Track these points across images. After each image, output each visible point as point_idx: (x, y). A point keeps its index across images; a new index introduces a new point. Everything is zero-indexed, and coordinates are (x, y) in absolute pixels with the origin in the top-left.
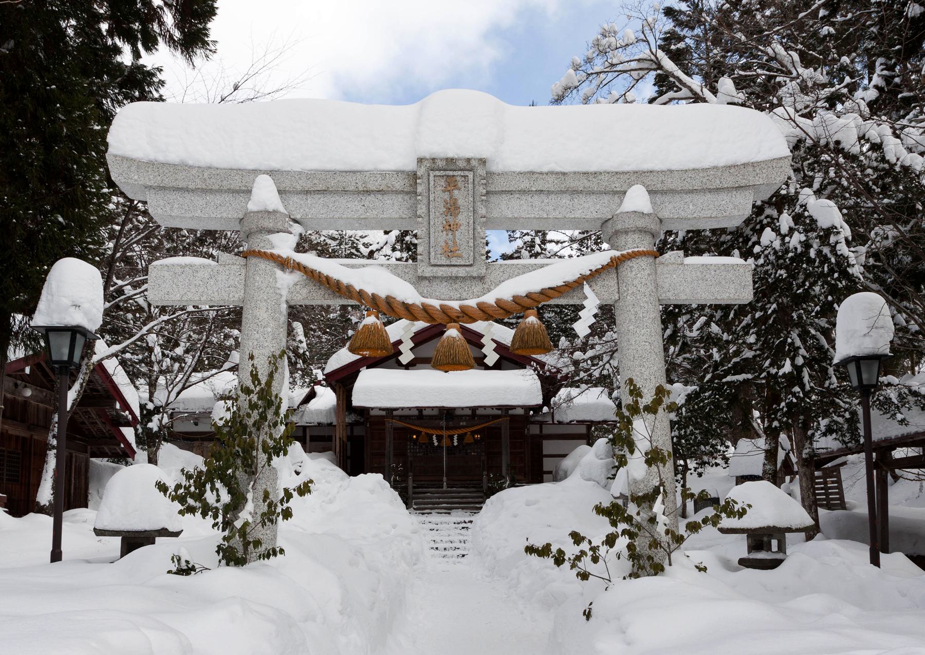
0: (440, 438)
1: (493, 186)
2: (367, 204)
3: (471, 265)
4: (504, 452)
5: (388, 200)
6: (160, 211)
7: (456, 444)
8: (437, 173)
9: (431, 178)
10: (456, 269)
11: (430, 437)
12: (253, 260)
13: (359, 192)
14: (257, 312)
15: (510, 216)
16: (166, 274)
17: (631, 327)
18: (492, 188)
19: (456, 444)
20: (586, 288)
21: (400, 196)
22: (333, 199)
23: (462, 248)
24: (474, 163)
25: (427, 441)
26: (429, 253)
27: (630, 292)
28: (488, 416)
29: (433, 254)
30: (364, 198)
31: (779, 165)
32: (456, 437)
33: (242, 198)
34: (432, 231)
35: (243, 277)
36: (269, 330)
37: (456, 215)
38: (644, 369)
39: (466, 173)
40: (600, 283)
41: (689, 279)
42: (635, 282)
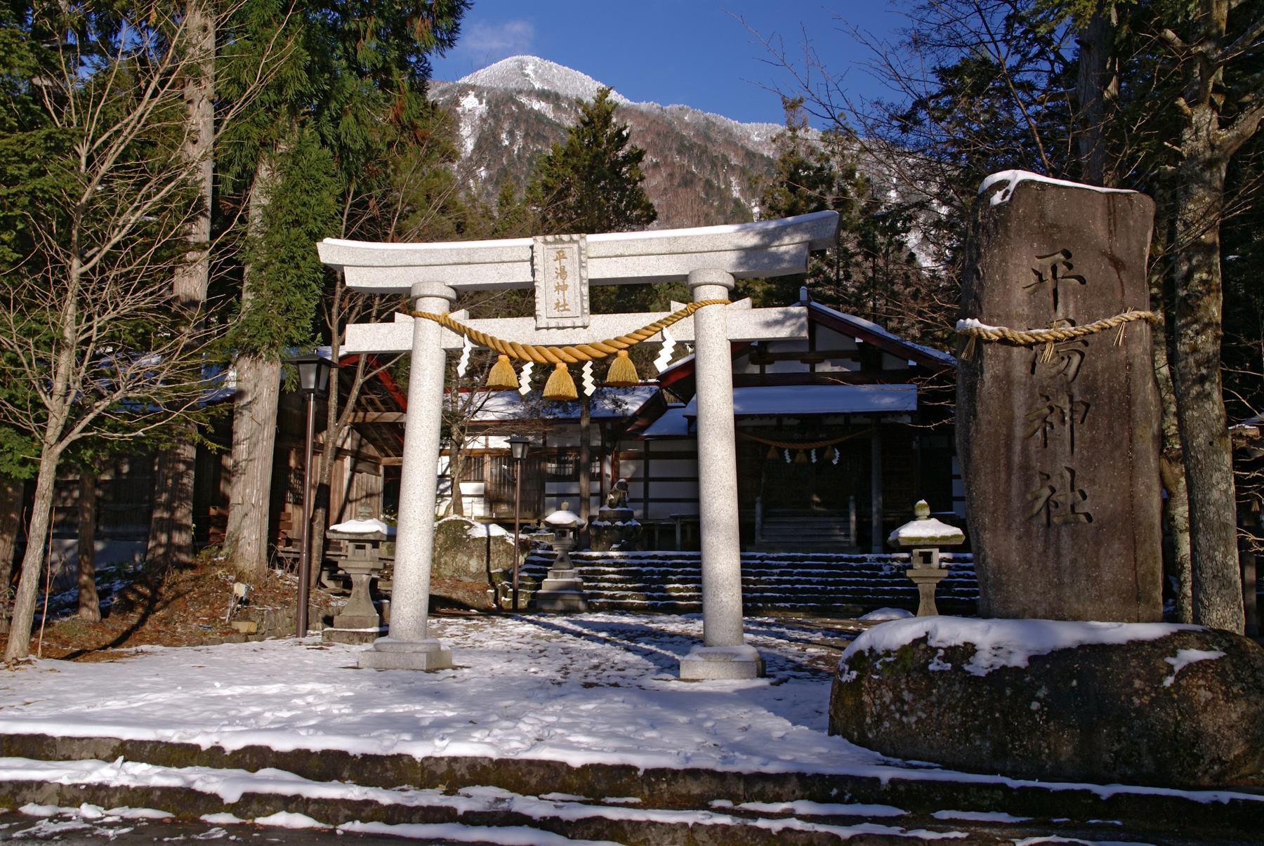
7: (814, 460)
19: (814, 460)
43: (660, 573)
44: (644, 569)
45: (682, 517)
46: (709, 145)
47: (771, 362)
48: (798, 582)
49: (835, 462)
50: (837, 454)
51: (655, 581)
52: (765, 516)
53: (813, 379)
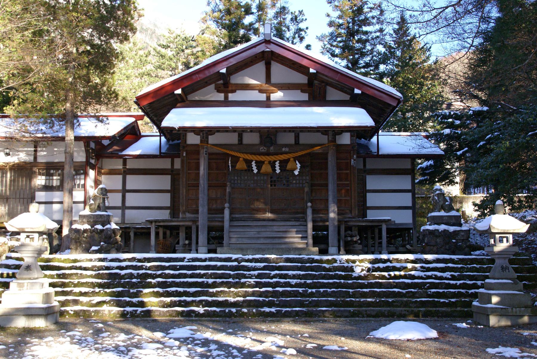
0: (259, 164)
7: (278, 171)
11: (248, 162)
19: (278, 171)
43: (139, 276)
44: (123, 272)
45: (156, 221)
46: (156, 29)
47: (233, 91)
48: (277, 284)
49: (296, 173)
50: (299, 165)
51: (134, 285)
52: (232, 220)
53: (268, 104)
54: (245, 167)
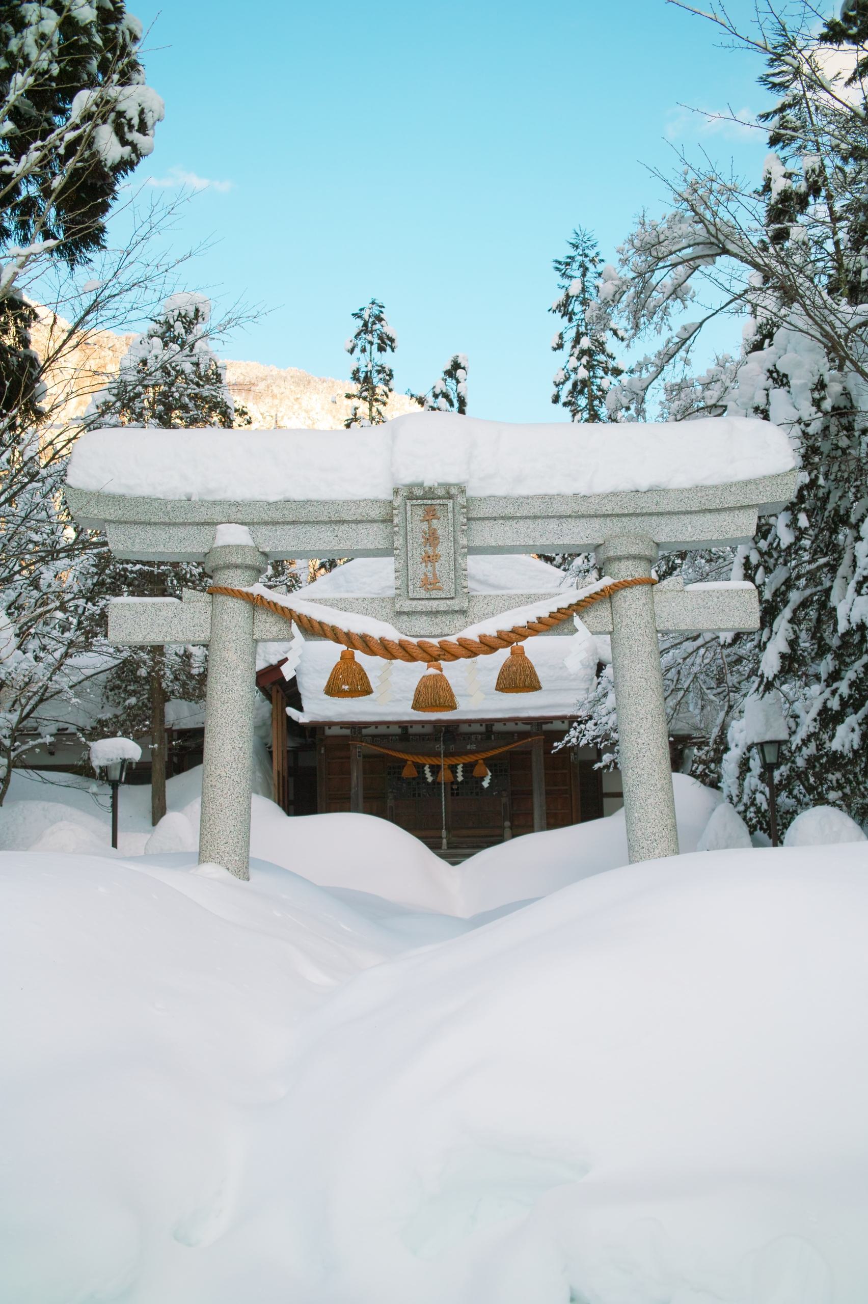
0: (435, 770)
1: (475, 513)
2: (340, 534)
3: (452, 598)
4: (535, 786)
5: (362, 529)
6: (121, 547)
7: (460, 779)
8: (414, 502)
9: (409, 508)
10: (437, 602)
11: (420, 768)
12: (221, 598)
13: (331, 522)
14: (225, 654)
15: (494, 544)
16: (128, 614)
17: (626, 662)
18: (474, 514)
19: (460, 779)
20: (577, 620)
21: (375, 525)
22: (304, 530)
23: (443, 579)
24: (453, 491)
25: (415, 774)
26: (408, 586)
27: (624, 624)
28: (511, 734)
29: (411, 587)
30: (336, 528)
31: (785, 481)
32: (460, 769)
33: (206, 530)
34: (410, 563)
35: (209, 615)
36: (239, 672)
37: (435, 546)
38: (639, 708)
39: (445, 501)
40: (592, 614)
41: (690, 607)
42: (629, 613)
47: (849, 517)
49: (486, 784)
54: (414, 773)
